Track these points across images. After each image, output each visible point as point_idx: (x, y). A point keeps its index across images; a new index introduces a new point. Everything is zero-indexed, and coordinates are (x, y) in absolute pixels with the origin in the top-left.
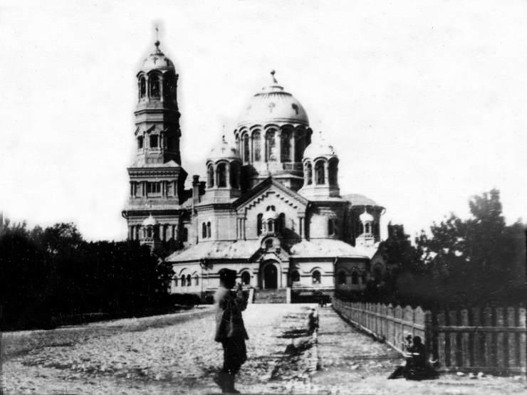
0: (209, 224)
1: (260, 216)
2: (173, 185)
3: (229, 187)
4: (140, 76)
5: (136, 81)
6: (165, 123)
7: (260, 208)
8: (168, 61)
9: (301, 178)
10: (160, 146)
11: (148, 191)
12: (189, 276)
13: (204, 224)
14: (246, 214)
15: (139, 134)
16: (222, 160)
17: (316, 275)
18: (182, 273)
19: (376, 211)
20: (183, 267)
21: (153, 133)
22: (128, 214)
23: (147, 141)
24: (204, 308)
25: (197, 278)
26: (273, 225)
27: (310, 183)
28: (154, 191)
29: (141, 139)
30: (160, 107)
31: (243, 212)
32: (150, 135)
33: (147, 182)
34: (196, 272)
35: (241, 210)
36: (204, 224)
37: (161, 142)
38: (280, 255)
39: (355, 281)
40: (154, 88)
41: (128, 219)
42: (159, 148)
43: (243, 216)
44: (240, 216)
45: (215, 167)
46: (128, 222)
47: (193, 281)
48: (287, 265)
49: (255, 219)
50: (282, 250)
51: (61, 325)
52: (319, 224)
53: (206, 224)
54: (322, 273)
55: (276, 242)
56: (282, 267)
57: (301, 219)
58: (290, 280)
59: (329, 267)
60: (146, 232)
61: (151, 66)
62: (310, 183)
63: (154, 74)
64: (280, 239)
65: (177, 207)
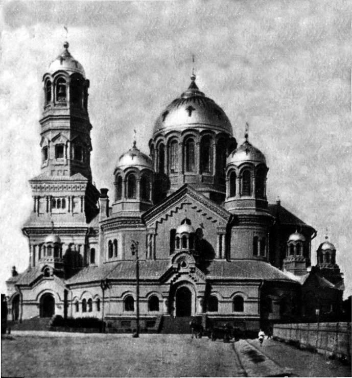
0: (116, 241)
1: (173, 232)
2: (79, 200)
3: (138, 199)
4: (46, 79)
5: (43, 84)
6: (73, 130)
7: (172, 223)
8: (76, 63)
9: (224, 193)
10: (66, 157)
11: (53, 206)
12: (90, 300)
13: (110, 241)
14: (156, 229)
15: (44, 145)
16: (131, 167)
17: (238, 303)
18: (84, 297)
19: (308, 232)
20: (85, 289)
21: (58, 142)
22: (28, 231)
23: (52, 151)
24: (131, 315)
25: (98, 302)
26: (188, 241)
27: (233, 194)
28: (58, 207)
29: (45, 150)
30: (68, 113)
31: (154, 226)
32: (55, 144)
33: (51, 197)
34: (97, 295)
35: (151, 224)
36: (110, 241)
37: (68, 151)
38: (195, 275)
40: (60, 92)
41: (29, 237)
42: (64, 159)
43: (154, 231)
44: (151, 232)
45: (123, 175)
46: (30, 240)
47: (94, 306)
48: (203, 288)
49: (168, 235)
50: (198, 270)
51: (308, 244)
52: (241, 240)
54: (245, 299)
55: (190, 261)
56: (197, 291)
57: (221, 235)
58: (58, 153)
59: (254, 292)
60: (46, 249)
61: (57, 66)
62: (233, 194)
63: (59, 77)
64: (196, 258)
65: (85, 225)
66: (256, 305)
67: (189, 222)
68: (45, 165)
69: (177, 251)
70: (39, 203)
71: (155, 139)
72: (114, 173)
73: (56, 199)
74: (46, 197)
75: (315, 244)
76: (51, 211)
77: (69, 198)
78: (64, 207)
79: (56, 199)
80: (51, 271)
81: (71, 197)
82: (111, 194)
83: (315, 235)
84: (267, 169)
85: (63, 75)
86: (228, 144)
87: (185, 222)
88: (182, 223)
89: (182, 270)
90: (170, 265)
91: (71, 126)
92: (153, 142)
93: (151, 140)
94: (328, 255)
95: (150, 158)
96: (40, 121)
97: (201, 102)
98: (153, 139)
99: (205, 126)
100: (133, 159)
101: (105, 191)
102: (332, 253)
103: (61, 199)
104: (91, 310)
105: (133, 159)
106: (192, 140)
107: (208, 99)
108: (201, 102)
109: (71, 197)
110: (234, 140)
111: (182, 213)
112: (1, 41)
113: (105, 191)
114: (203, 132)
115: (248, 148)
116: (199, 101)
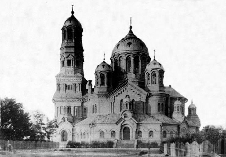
17: (151, 133)
19: (183, 100)
29: (63, 62)
30: (73, 44)
37: (73, 63)
55: (129, 114)
66: (74, 44)
67: (129, 97)
68: (62, 69)
69: (123, 110)
70: (60, 87)
71: (113, 57)
72: (95, 74)
73: (68, 85)
74: (63, 84)
75: (187, 105)
76: (65, 91)
77: (74, 85)
78: (71, 89)
79: (68, 85)
80: (66, 119)
81: (75, 84)
82: (94, 83)
83: (187, 101)
84: (82, 30)
85: (69, 28)
86: (146, 59)
87: (127, 97)
88: (126, 97)
89: (126, 119)
90: (121, 116)
91: (75, 51)
92: (112, 58)
93: (111, 57)
94: (192, 110)
95: (111, 66)
96: (60, 48)
97: (134, 40)
98: (112, 57)
99: (138, 52)
100: (103, 67)
101: (90, 82)
102: (195, 109)
103: (70, 85)
104: (84, 138)
105: (103, 67)
106: (130, 58)
107: (141, 41)
108: (134, 40)
109: (75, 84)
110: (149, 57)
111: (125, 93)
112: (67, 156)
113: (90, 82)
114: (135, 54)
115: (155, 62)
116: (133, 40)
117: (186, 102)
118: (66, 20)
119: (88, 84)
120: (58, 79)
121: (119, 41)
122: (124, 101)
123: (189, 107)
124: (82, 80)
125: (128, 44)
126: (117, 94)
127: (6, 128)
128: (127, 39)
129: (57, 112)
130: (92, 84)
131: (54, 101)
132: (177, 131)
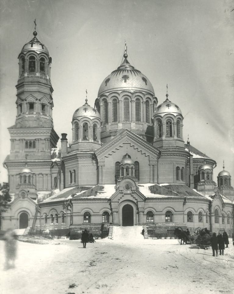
39: (200, 220)
53: (136, 275)
83: (216, 166)
101: (64, 135)
113: (64, 135)
116: (134, 72)
117: (215, 167)
118: (112, 71)
119: (61, 139)
120: (12, 132)
121: (108, 75)
122: (71, 171)
123: (219, 174)
124: (51, 134)
125: (122, 77)
126: (146, 153)
127: (1, 198)
128: (122, 71)
129: (76, 177)
130: (67, 139)
131: (5, 166)
132: (207, 210)
